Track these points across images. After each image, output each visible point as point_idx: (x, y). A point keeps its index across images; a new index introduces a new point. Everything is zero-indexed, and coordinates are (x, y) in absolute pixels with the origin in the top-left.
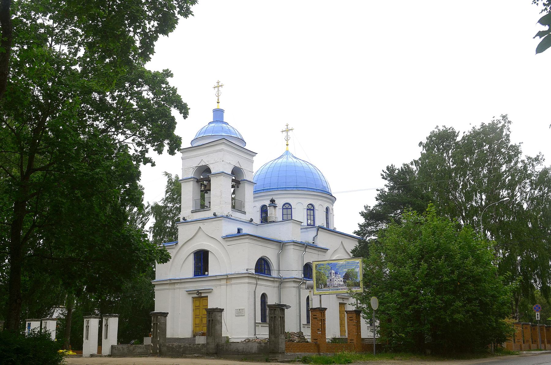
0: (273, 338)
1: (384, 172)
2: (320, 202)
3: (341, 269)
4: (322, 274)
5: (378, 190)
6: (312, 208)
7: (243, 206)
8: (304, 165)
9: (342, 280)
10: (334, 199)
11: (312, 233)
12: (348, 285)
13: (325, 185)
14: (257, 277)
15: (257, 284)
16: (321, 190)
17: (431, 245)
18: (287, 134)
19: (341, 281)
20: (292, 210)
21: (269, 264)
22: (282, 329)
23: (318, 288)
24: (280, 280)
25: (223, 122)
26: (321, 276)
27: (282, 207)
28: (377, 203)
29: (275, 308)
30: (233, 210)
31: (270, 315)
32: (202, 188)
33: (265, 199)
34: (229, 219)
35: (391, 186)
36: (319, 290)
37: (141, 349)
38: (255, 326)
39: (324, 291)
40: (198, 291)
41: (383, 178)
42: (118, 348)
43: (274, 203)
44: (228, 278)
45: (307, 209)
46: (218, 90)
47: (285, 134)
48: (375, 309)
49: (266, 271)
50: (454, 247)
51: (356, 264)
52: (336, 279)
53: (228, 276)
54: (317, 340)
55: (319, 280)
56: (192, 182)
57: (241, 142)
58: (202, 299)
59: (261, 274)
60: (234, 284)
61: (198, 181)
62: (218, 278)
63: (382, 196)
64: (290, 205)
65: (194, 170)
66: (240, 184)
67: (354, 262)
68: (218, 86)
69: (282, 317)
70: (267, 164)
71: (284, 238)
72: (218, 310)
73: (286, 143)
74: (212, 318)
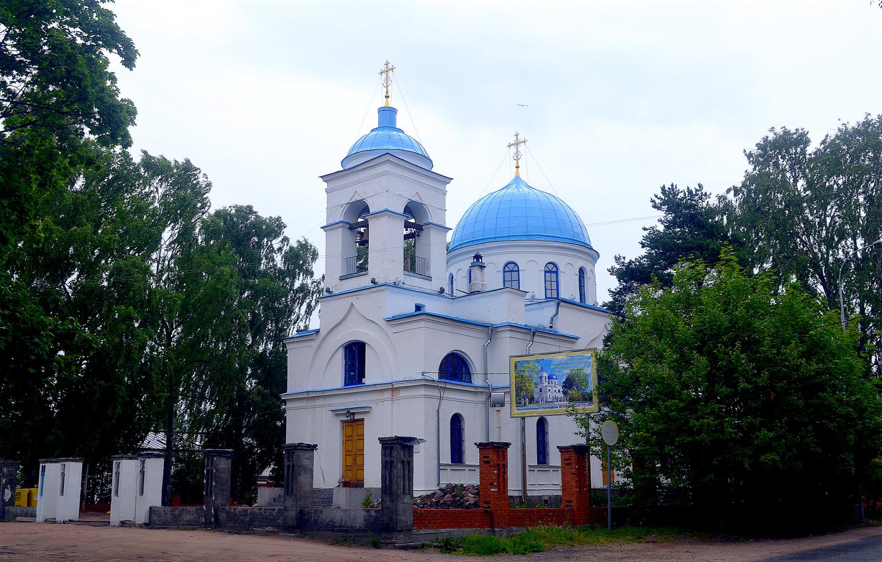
0: (388, 503)
1: (658, 199)
2: (567, 259)
3: (558, 370)
4: (525, 380)
5: (645, 229)
6: (555, 269)
7: (428, 266)
8: (553, 200)
9: (561, 390)
10: (596, 256)
11: (549, 310)
12: (572, 400)
13: (578, 230)
15: (441, 398)
16: (569, 239)
17: (716, 321)
18: (517, 150)
19: (559, 391)
20: (519, 274)
22: (407, 484)
23: (518, 404)
24: (487, 391)
26: (525, 383)
28: (643, 252)
29: (392, 445)
30: (406, 273)
31: (384, 458)
32: (358, 238)
34: (397, 289)
35: (668, 221)
36: (521, 408)
37: (190, 514)
38: (439, 470)
39: (529, 411)
40: (349, 411)
41: (655, 207)
42: (158, 511)
44: (393, 389)
45: (546, 272)
46: (387, 75)
47: (513, 149)
48: (611, 444)
50: (763, 324)
51: (586, 360)
52: (550, 388)
53: (393, 385)
54: (489, 503)
56: (341, 229)
57: (421, 159)
58: (355, 424)
59: (452, 382)
60: (404, 398)
61: (352, 227)
62: (378, 389)
63: (653, 240)
64: (516, 265)
66: (422, 230)
67: (582, 357)
68: (387, 70)
69: (406, 461)
70: (480, 200)
71: (495, 319)
72: (302, 448)
73: (514, 163)
74: (292, 461)
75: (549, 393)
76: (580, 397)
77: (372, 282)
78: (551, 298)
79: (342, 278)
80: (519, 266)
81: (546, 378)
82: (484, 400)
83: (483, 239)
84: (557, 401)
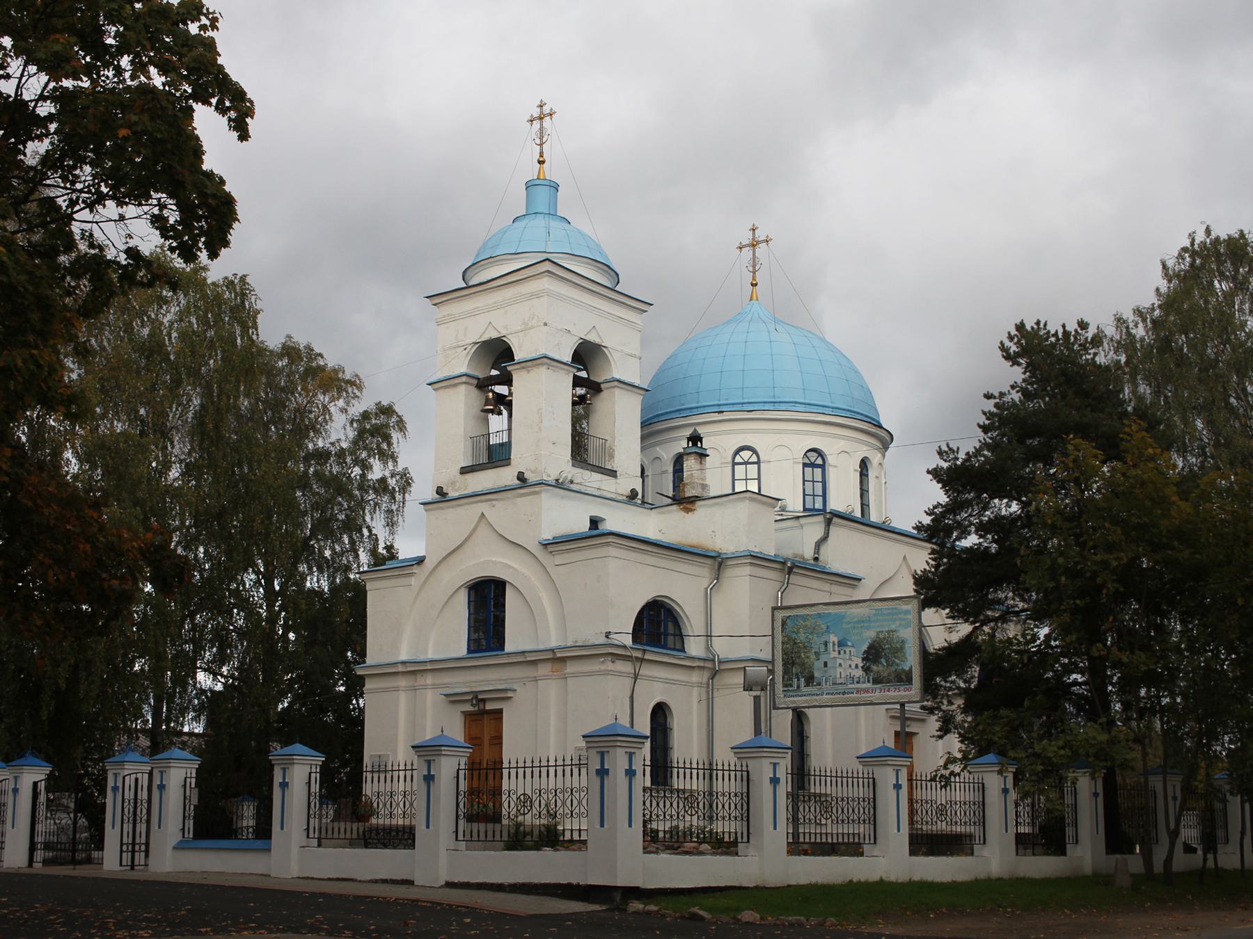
2: (842, 444)
5: (988, 396)
6: (819, 461)
15: (636, 676)
18: (754, 254)
19: (857, 666)
21: (679, 620)
24: (709, 665)
27: (730, 459)
34: (562, 491)
40: (477, 696)
43: (699, 445)
44: (557, 659)
45: (805, 465)
46: (541, 125)
49: (670, 638)
55: (793, 664)
56: (463, 387)
59: (653, 649)
60: (575, 675)
61: (483, 385)
62: (528, 659)
65: (468, 353)
67: (895, 611)
71: (723, 543)
75: (839, 670)
76: (892, 677)
77: (518, 479)
78: (814, 510)
79: (464, 471)
80: (760, 454)
81: (834, 645)
82: (705, 680)
83: (697, 408)
84: (853, 683)
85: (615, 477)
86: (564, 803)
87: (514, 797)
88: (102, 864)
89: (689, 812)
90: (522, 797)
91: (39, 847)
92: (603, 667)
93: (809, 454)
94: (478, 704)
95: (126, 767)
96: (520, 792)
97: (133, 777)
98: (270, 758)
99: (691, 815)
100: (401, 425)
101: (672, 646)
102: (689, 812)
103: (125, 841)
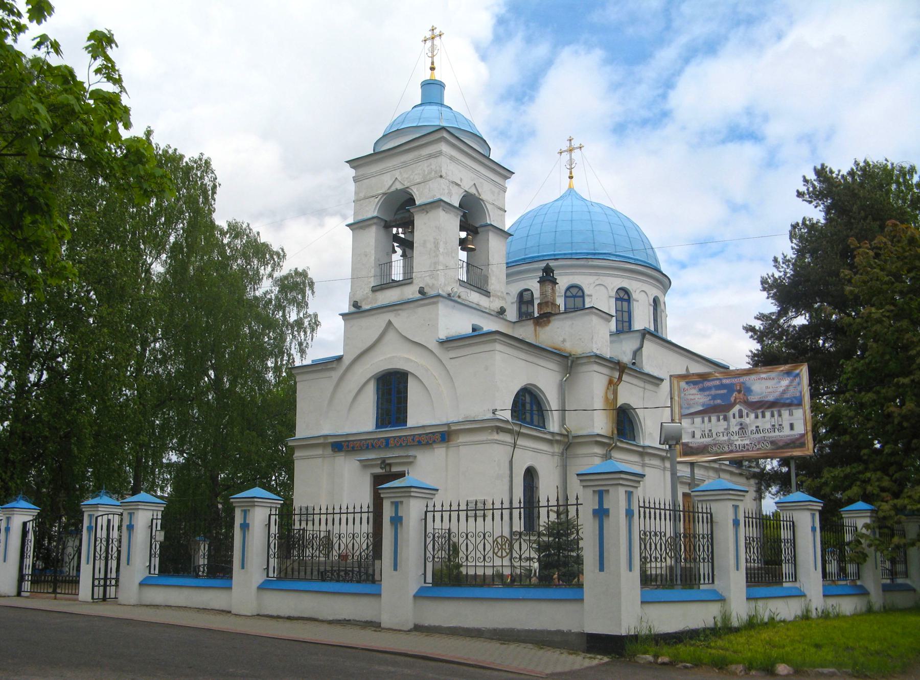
2: (646, 287)
6: (626, 297)
14: (516, 428)
18: (571, 156)
21: (541, 403)
25: (442, 105)
33: (528, 278)
45: (617, 299)
46: (433, 43)
47: (566, 156)
60: (465, 444)
68: (434, 36)
71: (573, 347)
79: (375, 289)
85: (489, 297)
86: (476, 547)
87: (491, 540)
88: (78, 595)
89: (499, 554)
90: (499, 540)
91: (26, 578)
92: (490, 437)
93: (619, 291)
94: (385, 468)
95: (100, 509)
96: (497, 533)
97: (105, 517)
98: (231, 500)
99: (502, 557)
100: (312, 285)
101: (537, 424)
102: (499, 554)
103: (97, 576)
